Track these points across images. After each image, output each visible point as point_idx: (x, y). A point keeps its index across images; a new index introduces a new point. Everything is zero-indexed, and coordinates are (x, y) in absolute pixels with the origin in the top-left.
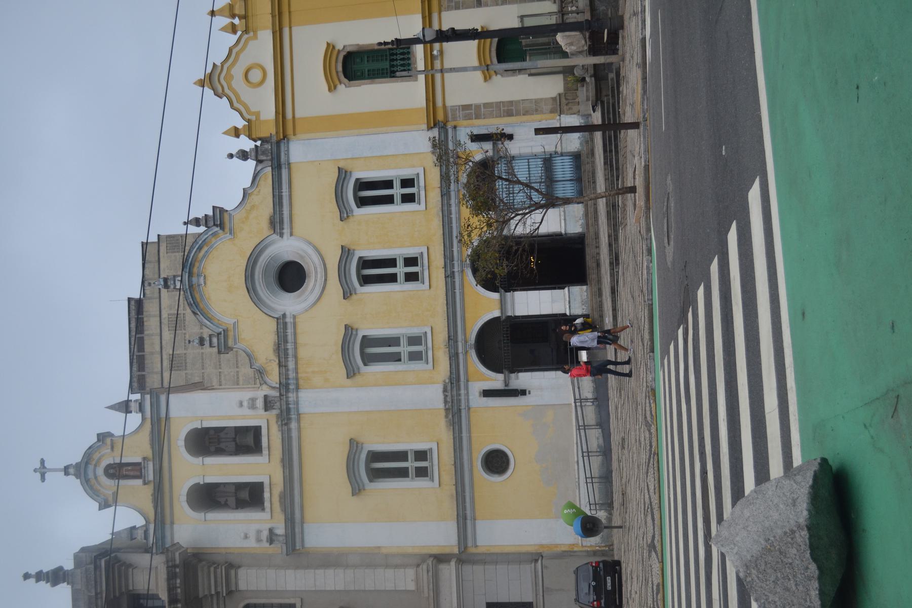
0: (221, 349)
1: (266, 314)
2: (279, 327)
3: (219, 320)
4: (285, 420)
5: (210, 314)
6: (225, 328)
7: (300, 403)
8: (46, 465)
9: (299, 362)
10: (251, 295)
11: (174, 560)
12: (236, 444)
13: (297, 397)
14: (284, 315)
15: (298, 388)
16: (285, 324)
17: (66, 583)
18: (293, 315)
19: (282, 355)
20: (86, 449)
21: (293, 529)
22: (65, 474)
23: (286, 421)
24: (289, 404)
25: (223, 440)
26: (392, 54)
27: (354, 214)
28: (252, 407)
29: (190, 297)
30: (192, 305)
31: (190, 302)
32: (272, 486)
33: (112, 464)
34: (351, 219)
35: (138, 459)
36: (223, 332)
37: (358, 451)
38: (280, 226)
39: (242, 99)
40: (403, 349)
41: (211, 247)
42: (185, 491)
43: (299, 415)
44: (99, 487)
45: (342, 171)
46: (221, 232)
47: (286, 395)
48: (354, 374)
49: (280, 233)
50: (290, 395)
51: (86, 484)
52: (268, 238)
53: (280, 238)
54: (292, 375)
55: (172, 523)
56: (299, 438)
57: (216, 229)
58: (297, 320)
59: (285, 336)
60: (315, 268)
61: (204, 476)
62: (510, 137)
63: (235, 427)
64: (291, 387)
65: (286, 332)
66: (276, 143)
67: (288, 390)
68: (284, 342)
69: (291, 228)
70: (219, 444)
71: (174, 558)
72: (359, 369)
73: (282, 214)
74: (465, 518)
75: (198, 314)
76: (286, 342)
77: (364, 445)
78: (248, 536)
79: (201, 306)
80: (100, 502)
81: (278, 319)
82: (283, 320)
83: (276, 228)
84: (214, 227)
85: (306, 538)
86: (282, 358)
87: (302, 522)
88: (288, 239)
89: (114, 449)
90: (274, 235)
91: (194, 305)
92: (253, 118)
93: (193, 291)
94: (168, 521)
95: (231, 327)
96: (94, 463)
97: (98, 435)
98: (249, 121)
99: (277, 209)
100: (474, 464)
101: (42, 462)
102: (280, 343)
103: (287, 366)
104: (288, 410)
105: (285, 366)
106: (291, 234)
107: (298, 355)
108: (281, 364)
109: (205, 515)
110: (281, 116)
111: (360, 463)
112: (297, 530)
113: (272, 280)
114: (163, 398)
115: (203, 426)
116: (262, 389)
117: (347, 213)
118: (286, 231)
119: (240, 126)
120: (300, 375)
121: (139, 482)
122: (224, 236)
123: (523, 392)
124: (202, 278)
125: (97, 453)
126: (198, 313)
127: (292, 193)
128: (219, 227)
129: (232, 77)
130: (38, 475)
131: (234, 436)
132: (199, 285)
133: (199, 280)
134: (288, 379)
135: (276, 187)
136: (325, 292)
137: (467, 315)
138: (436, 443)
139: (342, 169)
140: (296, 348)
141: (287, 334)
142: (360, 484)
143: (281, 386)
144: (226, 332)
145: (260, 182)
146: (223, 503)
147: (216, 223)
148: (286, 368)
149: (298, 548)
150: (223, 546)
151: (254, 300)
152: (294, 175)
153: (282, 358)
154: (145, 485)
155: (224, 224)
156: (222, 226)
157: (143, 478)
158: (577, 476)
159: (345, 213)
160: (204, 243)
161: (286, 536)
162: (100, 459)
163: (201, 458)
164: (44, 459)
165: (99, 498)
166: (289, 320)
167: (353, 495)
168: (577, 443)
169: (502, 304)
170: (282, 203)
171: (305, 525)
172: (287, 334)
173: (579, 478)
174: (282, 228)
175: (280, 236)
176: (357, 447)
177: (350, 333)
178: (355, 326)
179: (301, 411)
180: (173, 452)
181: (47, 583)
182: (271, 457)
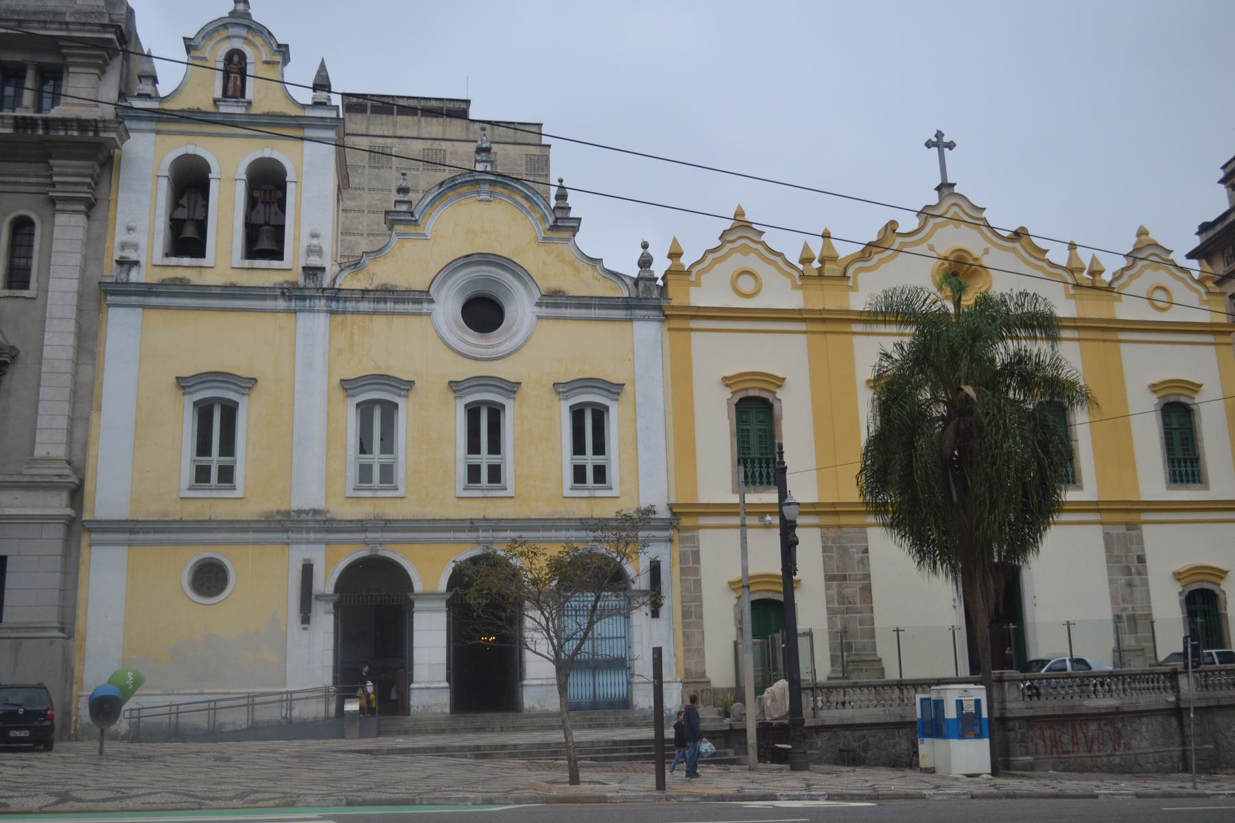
1: (436, 277)
2: (417, 293)
9: (367, 318)
10: (462, 260)
11: (106, 130)
13: (319, 311)
14: (431, 301)
15: (332, 312)
16: (420, 302)
24: (310, 299)
27: (562, 402)
29: (464, 180)
30: (453, 181)
32: (198, 269)
33: (245, 61)
34: (556, 397)
35: (249, 95)
36: (414, 219)
41: (528, 212)
43: (295, 312)
44: (215, 40)
45: (618, 389)
46: (548, 226)
50: (323, 302)
54: (350, 306)
55: (158, 132)
58: (424, 317)
59: (403, 301)
60: (492, 346)
62: (655, 614)
64: (334, 305)
67: (329, 299)
69: (547, 318)
70: (262, 202)
72: (353, 396)
74: (131, 531)
75: (440, 188)
76: (396, 301)
78: (131, 232)
79: (451, 194)
84: (554, 218)
87: (144, 307)
88: (534, 313)
89: (265, 65)
92: (693, 278)
95: (419, 230)
96: (250, 37)
97: (286, 46)
98: (689, 272)
103: (363, 300)
105: (362, 298)
107: (376, 316)
108: (366, 293)
110: (693, 313)
112: (134, 299)
113: (481, 289)
114: (331, 134)
117: (564, 392)
118: (544, 311)
119: (682, 260)
120: (349, 317)
121: (218, 93)
122: (541, 230)
125: (262, 42)
129: (746, 254)
134: (345, 301)
136: (460, 358)
137: (418, 547)
140: (386, 313)
142: (191, 390)
151: (455, 262)
152: (616, 326)
155: (558, 231)
156: (555, 227)
158: (181, 692)
163: (245, 177)
166: (425, 307)
171: (139, 310)
173: (178, 694)
174: (547, 305)
176: (245, 388)
178: (411, 395)
179: (300, 315)
182: (239, 270)
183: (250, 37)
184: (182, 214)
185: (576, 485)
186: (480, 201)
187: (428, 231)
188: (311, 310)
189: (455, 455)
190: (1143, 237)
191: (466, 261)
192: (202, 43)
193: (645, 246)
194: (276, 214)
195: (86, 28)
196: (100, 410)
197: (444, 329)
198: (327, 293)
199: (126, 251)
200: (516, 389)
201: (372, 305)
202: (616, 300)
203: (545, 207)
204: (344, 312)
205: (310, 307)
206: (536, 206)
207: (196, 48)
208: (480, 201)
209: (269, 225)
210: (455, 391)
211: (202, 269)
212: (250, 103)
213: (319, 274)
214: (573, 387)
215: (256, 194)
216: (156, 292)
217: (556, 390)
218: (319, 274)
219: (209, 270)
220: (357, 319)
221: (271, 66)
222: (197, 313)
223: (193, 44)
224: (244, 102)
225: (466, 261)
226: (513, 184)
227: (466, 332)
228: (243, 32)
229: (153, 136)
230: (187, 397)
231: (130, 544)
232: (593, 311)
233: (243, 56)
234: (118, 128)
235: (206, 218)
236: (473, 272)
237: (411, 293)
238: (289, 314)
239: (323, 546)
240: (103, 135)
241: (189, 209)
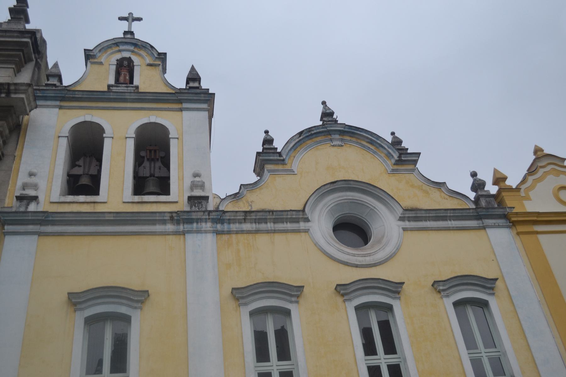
0: (263, 156)
1: (308, 201)
2: (294, 213)
3: (294, 157)
4: (177, 216)
5: (301, 149)
6: (287, 161)
7: (199, 235)
8: (135, 22)
9: (250, 236)
10: (328, 186)
11: (16, 91)
12: (148, 177)
13: (206, 232)
14: (307, 220)
15: (218, 233)
16: (297, 221)
17: (10, 18)
18: (309, 229)
19: (259, 216)
20: (150, 44)
21: (33, 222)
22: (125, 32)
23: (175, 218)
24: (197, 223)
25: (153, 165)
27: (444, 299)
28: (193, 184)
29: (318, 131)
30: (309, 131)
31: (313, 130)
32: (92, 205)
33: (133, 64)
34: (437, 296)
35: (136, 82)
36: (282, 158)
37: (129, 303)
38: (412, 217)
39: (538, 184)
40: (275, 365)
41: (375, 152)
42: (96, 120)
43: (184, 233)
44: (109, 53)
45: (492, 284)
46: (393, 161)
47: (209, 219)
48: (237, 299)
49: (404, 217)
50: (209, 225)
51: (114, 42)
53: (398, 218)
54: (234, 227)
55: (61, 107)
57: (396, 156)
58: (303, 234)
59: (282, 221)
60: (369, 255)
61: (113, 138)
63: (169, 178)
64: (219, 227)
65: (287, 222)
66: (504, 214)
67: (216, 221)
68: (274, 219)
69: (412, 229)
70: (148, 159)
71: (19, 93)
72: (246, 304)
73: (426, 220)
75: (300, 136)
76: (276, 221)
77: (139, 310)
78: (33, 177)
79: (309, 142)
80: (94, 51)
81: (303, 210)
82: (302, 218)
83: (410, 212)
84: (398, 154)
86: (256, 216)
87: (40, 234)
89: (149, 67)
90: (401, 210)
91: (310, 133)
92: (522, 193)
93: (324, 135)
95: (287, 167)
97: (165, 54)
98: (518, 189)
99: (432, 214)
101: (139, 19)
102: (274, 213)
103: (245, 222)
104: (190, 221)
105: (245, 219)
106: (405, 229)
107: (259, 235)
108: (248, 214)
109: (66, 137)
110: (535, 218)
112: (30, 228)
114: (205, 106)
115: (171, 140)
116: (215, 198)
117: (444, 290)
118: (407, 224)
119: (508, 182)
120: (234, 236)
121: (112, 81)
122: (390, 163)
124: (340, 143)
125: (146, 54)
126: (301, 137)
127: (451, 231)
128: (398, 159)
130: (126, 15)
131: (155, 176)
132: (331, 140)
133: (338, 140)
134: (229, 223)
135: (456, 213)
136: (341, 266)
139: (495, 283)
140: (268, 232)
141: (285, 223)
142: (83, 306)
143: (221, 213)
144: (282, 162)
145: (455, 199)
146: (77, 163)
147: (402, 156)
148: (243, 221)
149: (6, 227)
150: (21, 166)
151: (323, 188)
152: (472, 234)
153: (256, 216)
154: (108, 86)
155: (402, 165)
156: (400, 162)
157: (115, 85)
159: (444, 288)
160: (378, 146)
161: (26, 212)
162: (140, 55)
163: (134, 136)
164: (142, 21)
165: (97, 51)
166: (302, 225)
167: (69, 294)
170: (439, 220)
171: (36, 237)
172: (285, 223)
174: (409, 219)
175: (400, 217)
176: (138, 301)
177: (293, 293)
178: (301, 301)
179: (188, 236)
181: (14, 6)
182: (130, 204)
183: (136, 50)
184: (77, 171)
186: (333, 146)
187: (294, 168)
189: (355, 355)
191: (332, 187)
192: (99, 55)
193: (474, 175)
194: (160, 169)
195: (8, 34)
197: (322, 243)
198: (214, 215)
199: (26, 190)
200: (400, 289)
201: (254, 225)
202: (468, 211)
204: (229, 232)
205: (197, 228)
206: (381, 148)
207: (94, 57)
208: (333, 146)
209: (154, 176)
210: (343, 295)
211: (96, 204)
212: (137, 87)
213: (204, 202)
214: (451, 285)
215: (143, 154)
216: (52, 220)
217: (436, 289)
218: (204, 202)
219: (102, 205)
220: (242, 238)
221: (153, 67)
222: (91, 238)
224: (132, 87)
225: (332, 187)
226: (359, 132)
227: (342, 246)
228: (132, 48)
229: (57, 110)
230: (78, 313)
232: (449, 222)
233: (130, 60)
234: (27, 90)
235: (99, 171)
236: (339, 197)
237: (289, 213)
238: (178, 236)
240: (13, 96)
241: (84, 168)
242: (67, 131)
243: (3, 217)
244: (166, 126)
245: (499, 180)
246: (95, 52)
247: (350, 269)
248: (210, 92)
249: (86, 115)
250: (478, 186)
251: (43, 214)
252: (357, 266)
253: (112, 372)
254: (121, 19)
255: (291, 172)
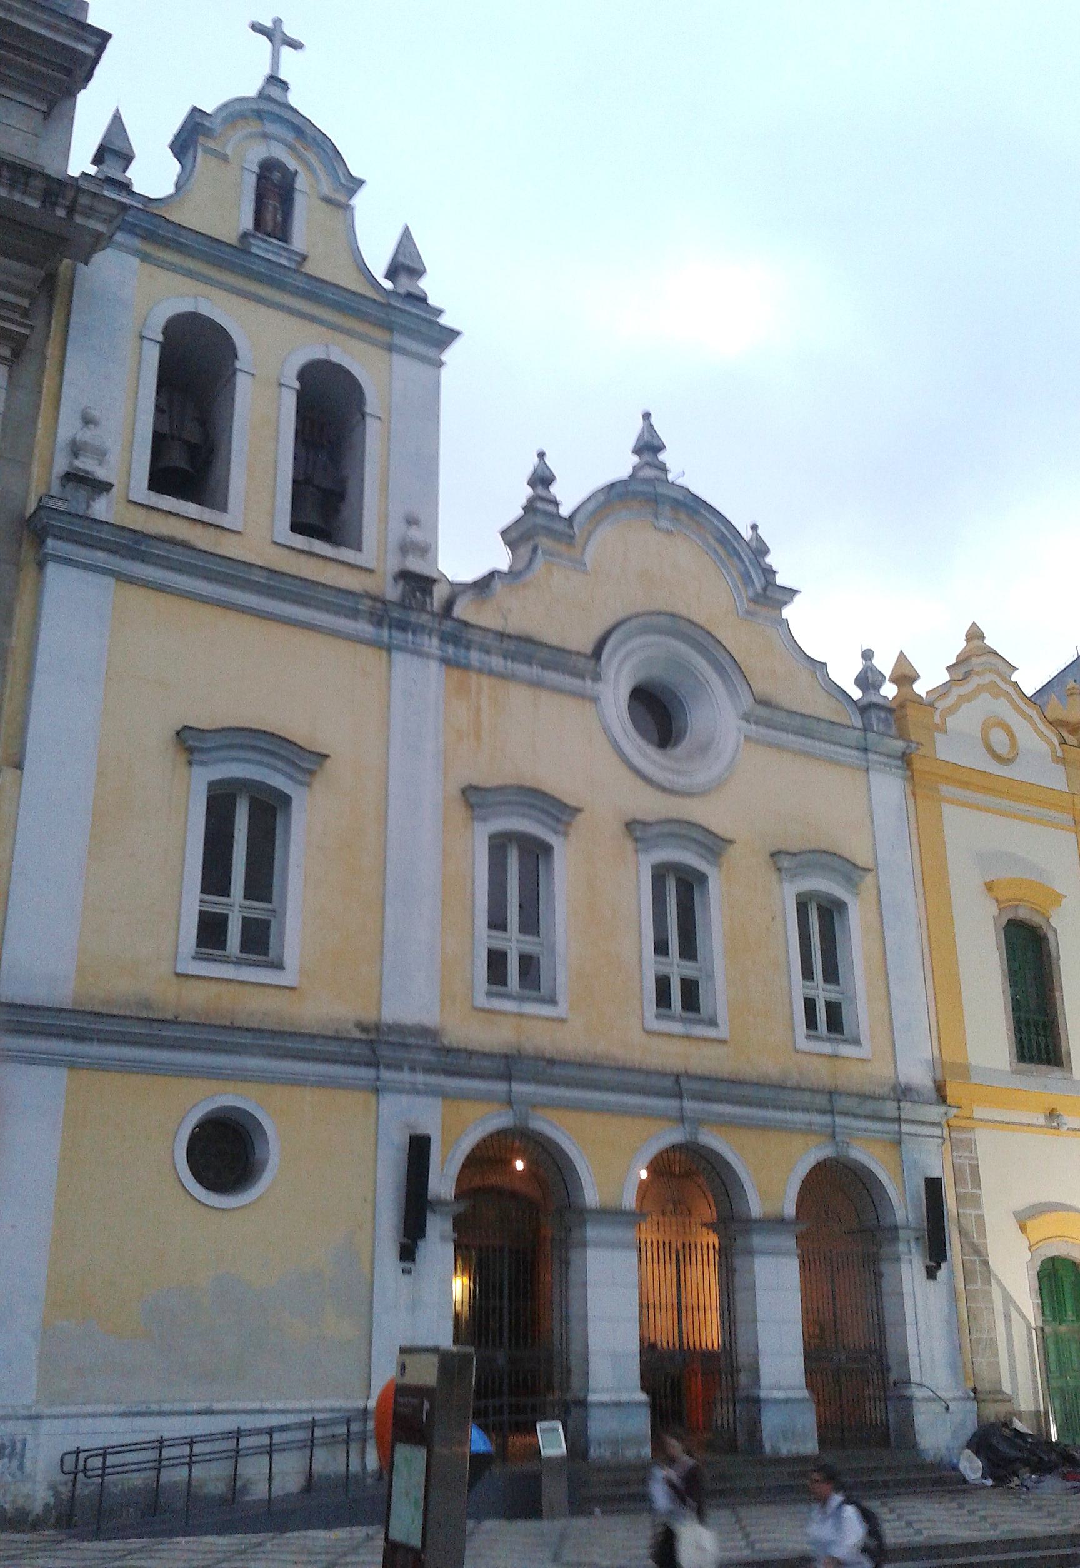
15: (445, 661)
26: (1045, 1027)
41: (724, 564)
46: (751, 593)
48: (471, 806)
52: (746, 688)
55: (145, 258)
56: (335, 633)
62: (931, 1274)
64: (451, 650)
72: (484, 819)
74: (79, 1036)
78: (91, 426)
85: (74, 573)
88: (739, 729)
89: (323, 204)
94: (149, 248)
96: (298, 146)
100: (230, 1086)
111: (265, 771)
113: (657, 673)
121: (248, 223)
123: (407, 1253)
129: (996, 696)
136: (640, 783)
137: (589, 1118)
138: (295, 985)
158: (167, 1407)
164: (300, 50)
168: (262, 1411)
169: (777, 1223)
171: (110, 581)
173: (161, 1414)
179: (398, 657)
180: (315, 329)
183: (298, 146)
185: (245, 956)
188: (418, 652)
189: (641, 952)
190: (976, 642)
196: (19, 766)
199: (82, 458)
203: (750, 560)
206: (736, 559)
219: (232, 536)
222: (218, 612)
223: (207, 124)
226: (707, 514)
228: (290, 136)
229: (135, 262)
230: (196, 769)
231: (73, 1064)
233: (289, 178)
239: (64, 1072)
240: (79, 219)
242: (160, 329)
243: (49, 518)
244: (343, 364)
245: (905, 676)
246: (216, 124)
247: (649, 790)
248: (769, 560)
249: (199, 298)
250: (868, 679)
251: (132, 536)
252: (663, 789)
253: (229, 896)
254: (257, 28)
255: (579, 564)
